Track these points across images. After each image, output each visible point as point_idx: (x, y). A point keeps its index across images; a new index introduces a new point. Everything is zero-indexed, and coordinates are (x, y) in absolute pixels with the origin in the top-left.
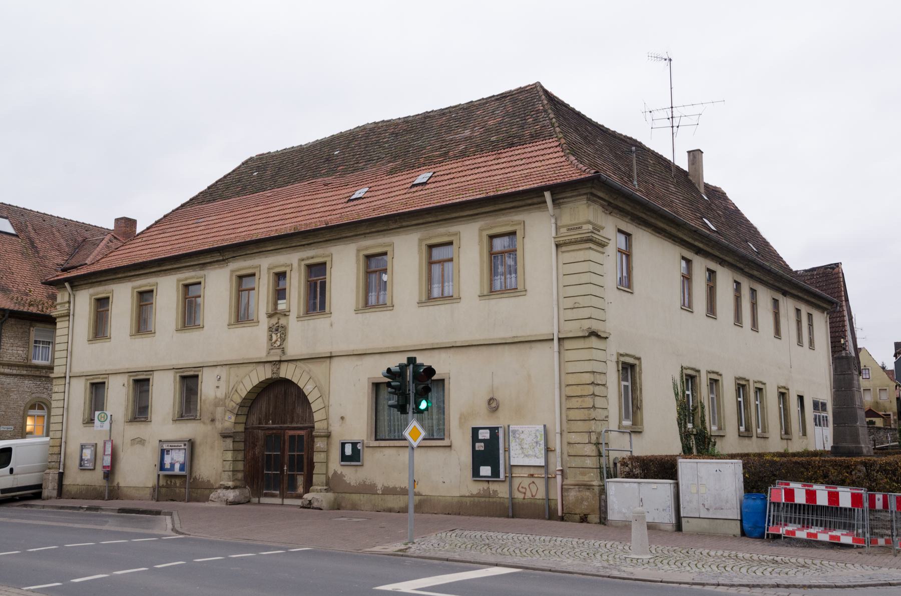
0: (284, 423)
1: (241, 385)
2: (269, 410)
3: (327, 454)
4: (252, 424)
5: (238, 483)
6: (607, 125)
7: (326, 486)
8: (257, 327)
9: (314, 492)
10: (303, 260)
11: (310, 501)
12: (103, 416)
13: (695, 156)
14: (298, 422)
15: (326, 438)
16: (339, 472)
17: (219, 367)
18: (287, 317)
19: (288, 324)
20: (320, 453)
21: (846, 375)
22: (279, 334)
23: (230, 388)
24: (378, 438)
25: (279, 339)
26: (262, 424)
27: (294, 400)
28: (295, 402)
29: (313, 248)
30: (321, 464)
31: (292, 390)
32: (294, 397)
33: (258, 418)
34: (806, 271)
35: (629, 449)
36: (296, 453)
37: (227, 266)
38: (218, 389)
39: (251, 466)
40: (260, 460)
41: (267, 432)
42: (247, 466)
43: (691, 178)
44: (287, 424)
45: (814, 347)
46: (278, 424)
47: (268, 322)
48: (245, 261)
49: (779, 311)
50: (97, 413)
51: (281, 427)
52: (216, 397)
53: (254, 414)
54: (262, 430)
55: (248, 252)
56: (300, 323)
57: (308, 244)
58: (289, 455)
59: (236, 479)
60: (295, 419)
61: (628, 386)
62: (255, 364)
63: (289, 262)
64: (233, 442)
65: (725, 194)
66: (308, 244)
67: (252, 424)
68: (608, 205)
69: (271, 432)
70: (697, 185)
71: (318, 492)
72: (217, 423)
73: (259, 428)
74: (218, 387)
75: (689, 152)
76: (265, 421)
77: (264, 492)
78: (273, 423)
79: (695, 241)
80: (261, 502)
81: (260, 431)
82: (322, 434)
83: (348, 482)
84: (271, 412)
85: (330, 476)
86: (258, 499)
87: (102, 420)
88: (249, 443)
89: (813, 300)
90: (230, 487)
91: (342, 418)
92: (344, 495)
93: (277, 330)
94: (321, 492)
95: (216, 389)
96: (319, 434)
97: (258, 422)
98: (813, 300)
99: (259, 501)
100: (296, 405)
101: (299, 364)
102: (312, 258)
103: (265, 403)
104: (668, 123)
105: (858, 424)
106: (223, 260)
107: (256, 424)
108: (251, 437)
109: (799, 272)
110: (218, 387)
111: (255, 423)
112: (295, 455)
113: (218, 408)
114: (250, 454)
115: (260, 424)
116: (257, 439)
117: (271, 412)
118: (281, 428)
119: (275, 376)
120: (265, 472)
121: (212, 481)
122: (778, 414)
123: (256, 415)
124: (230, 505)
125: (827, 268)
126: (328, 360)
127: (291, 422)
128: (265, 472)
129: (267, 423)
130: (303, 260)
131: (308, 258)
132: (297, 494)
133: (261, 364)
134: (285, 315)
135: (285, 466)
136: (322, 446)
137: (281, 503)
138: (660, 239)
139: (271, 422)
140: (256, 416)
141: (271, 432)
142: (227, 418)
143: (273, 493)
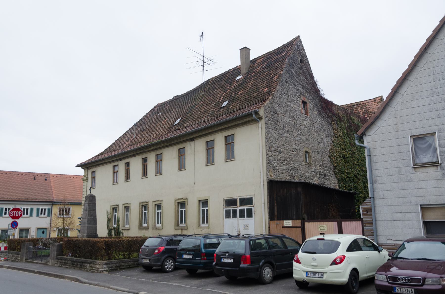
75: (240, 49)
89: (247, 120)
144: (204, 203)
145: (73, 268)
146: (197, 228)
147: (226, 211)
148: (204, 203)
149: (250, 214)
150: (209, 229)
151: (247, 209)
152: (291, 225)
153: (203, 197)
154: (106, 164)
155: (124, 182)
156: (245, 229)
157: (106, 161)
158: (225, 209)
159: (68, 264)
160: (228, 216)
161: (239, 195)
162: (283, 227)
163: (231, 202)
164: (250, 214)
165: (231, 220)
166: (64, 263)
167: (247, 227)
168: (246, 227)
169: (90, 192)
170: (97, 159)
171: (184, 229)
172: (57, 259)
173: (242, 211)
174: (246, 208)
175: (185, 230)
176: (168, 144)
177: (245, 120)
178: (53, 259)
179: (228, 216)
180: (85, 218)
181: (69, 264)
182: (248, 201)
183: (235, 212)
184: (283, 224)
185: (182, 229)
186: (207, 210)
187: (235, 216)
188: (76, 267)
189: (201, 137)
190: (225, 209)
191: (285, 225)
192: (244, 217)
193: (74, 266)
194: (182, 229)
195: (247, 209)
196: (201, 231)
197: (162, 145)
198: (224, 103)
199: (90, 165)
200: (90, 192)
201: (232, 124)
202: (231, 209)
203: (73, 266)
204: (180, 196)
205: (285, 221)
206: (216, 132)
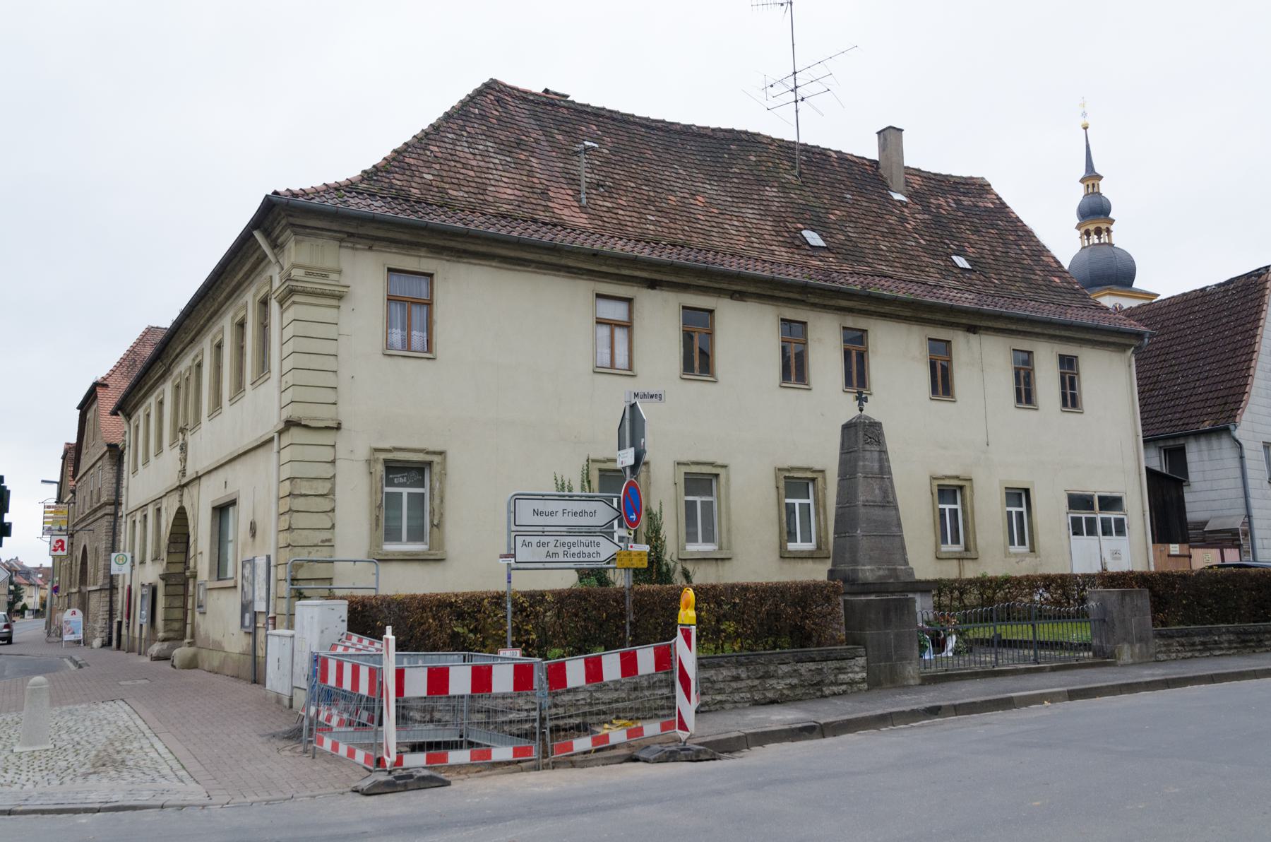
5: (171, 635)
6: (670, 118)
7: (378, 635)
12: (121, 558)
13: (890, 137)
21: (853, 454)
24: (221, 577)
34: (1219, 285)
35: (375, 587)
43: (882, 172)
45: (1082, 409)
49: (951, 357)
50: (114, 555)
59: (171, 630)
61: (423, 494)
64: (166, 585)
65: (989, 185)
68: (348, 236)
70: (889, 181)
75: (879, 133)
79: (618, 269)
87: (121, 562)
89: (1063, 333)
98: (1063, 333)
104: (792, 96)
105: (859, 532)
109: (1208, 289)
122: (1140, 513)
125: (1252, 276)
126: (197, 481)
144: (1019, 496)
145: (1248, 650)
146: (1005, 557)
147: (1072, 518)
148: (1019, 496)
149: (1121, 530)
150: (1038, 559)
151: (1115, 519)
152: (1178, 553)
153: (1019, 481)
154: (537, 268)
155: (778, 385)
156: (1115, 559)
157: (571, 263)
158: (1070, 515)
159: (1221, 643)
160: (1077, 529)
161: (1097, 487)
162: (1169, 556)
163: (1079, 502)
164: (1121, 530)
165: (1084, 541)
166: (1203, 643)
167: (1117, 555)
168: (1116, 554)
169: (861, 410)
170: (331, 202)
171: (967, 559)
172: (1161, 635)
173: (1105, 522)
174: (1112, 515)
175: (970, 561)
176: (908, 314)
177: (1112, 339)
178: (1141, 640)
179: (1077, 531)
180: (883, 506)
181: (1226, 645)
182: (1111, 503)
183: (1091, 522)
184: (1169, 550)
185: (959, 559)
186: (708, 507)
187: (1091, 532)
188: (1258, 647)
189: (998, 332)
190: (1070, 515)
191: (1172, 553)
192: (1111, 534)
193: (1251, 647)
194: (959, 559)
195: (1115, 519)
196: (1017, 563)
197: (887, 309)
198: (815, 235)
199: (752, 289)
200: (861, 410)
201: (1087, 337)
202: (1084, 515)
203: (1245, 647)
204: (949, 468)
205: (1171, 545)
206: (825, 307)
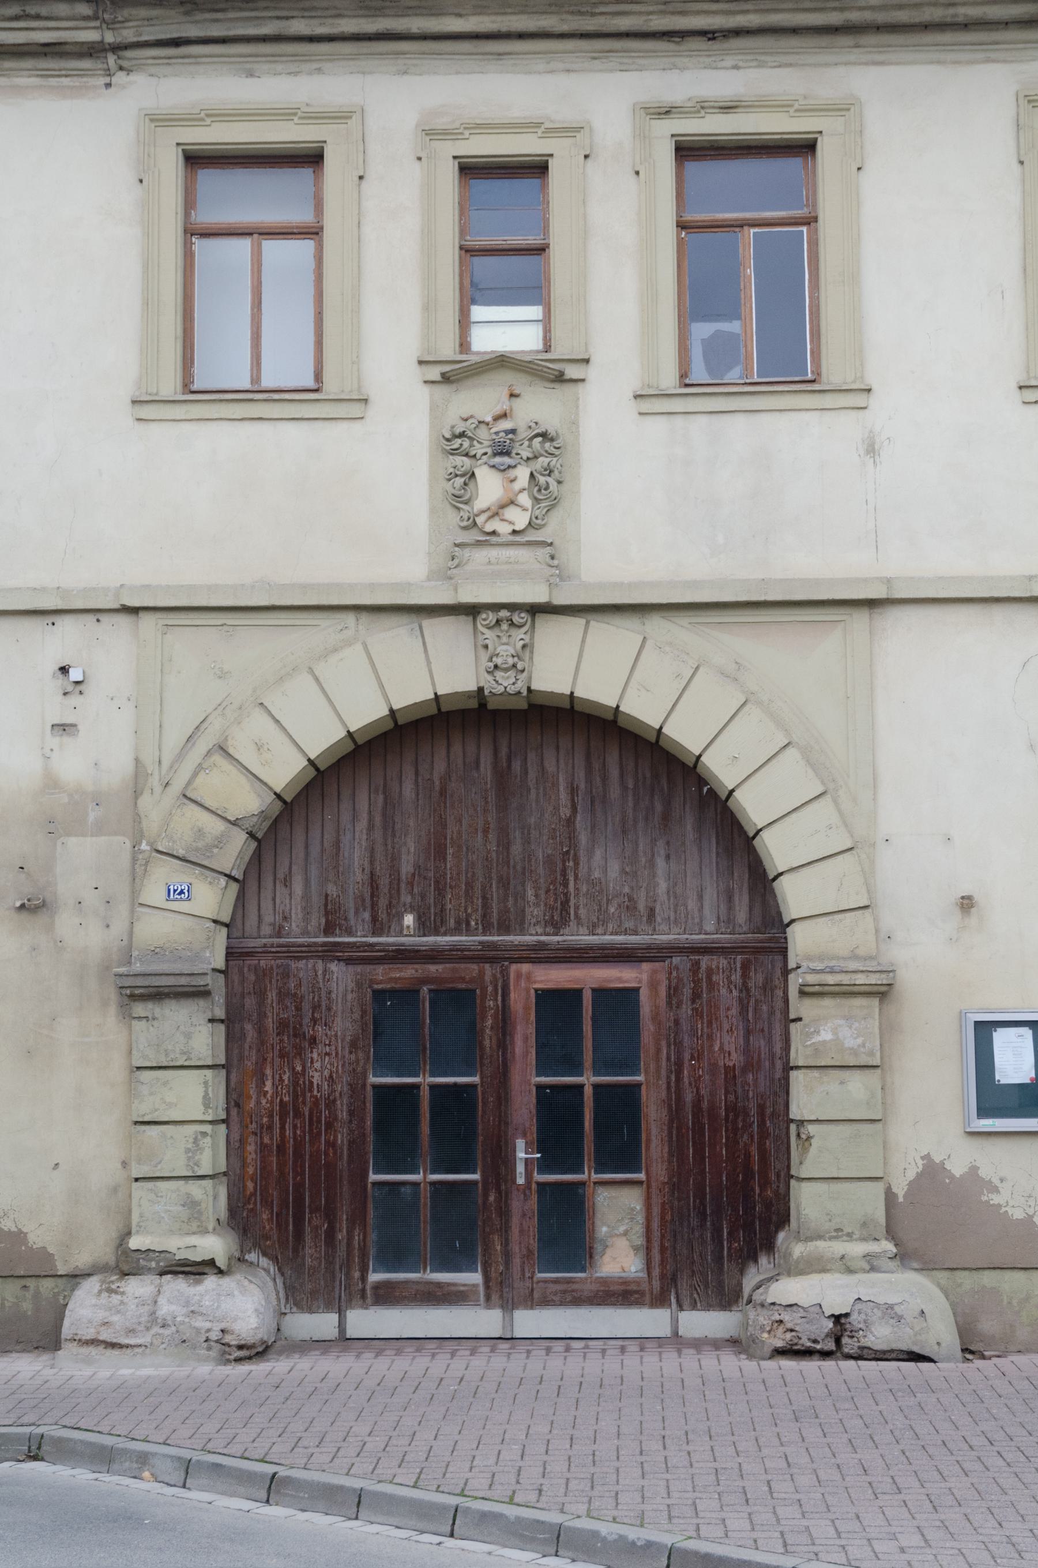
0: (505, 928)
1: (258, 725)
2: (394, 859)
3: (883, 1079)
4: (279, 933)
8: (357, 426)
9: (824, 1270)
10: (667, 112)
11: (837, 1319)
14: (605, 922)
15: (875, 1002)
16: (957, 1168)
17: (66, 624)
18: (568, 388)
19: (575, 423)
20: (846, 1074)
22: (522, 474)
23: (174, 738)
25: (524, 499)
26: (350, 932)
27: (565, 812)
28: (570, 822)
29: (729, 61)
30: (846, 1129)
31: (550, 766)
32: (564, 796)
33: (316, 900)
36: (425, 1080)
37: (108, 85)
38: (66, 739)
39: (281, 1149)
40: (343, 1115)
41: (380, 972)
42: (251, 1148)
44: (522, 932)
46: (462, 926)
47: (434, 408)
48: (251, 74)
51: (493, 946)
52: (51, 783)
53: (287, 882)
54: (349, 961)
55: (299, 26)
56: (658, 426)
57: (709, 35)
58: (540, 1087)
60: (582, 906)
62: (350, 618)
63: (563, 114)
66: (709, 35)
67: (279, 933)
69: (408, 972)
71: (850, 1271)
72: (66, 923)
73: (330, 952)
74: (63, 728)
76: (367, 915)
77: (374, 1277)
78: (424, 926)
80: (350, 1333)
81: (334, 967)
82: (861, 979)
83: (1018, 1214)
84: (406, 868)
85: (900, 1190)
86: (334, 1317)
88: (261, 1030)
90: (211, 1263)
91: (967, 904)
92: (988, 1279)
93: (502, 451)
94: (873, 1269)
95: (54, 741)
96: (845, 979)
97: (317, 920)
99: (675, 1322)
100: (583, 838)
101: (657, 626)
102: (727, 108)
103: (362, 824)
106: (92, 51)
107: (305, 933)
108: (272, 996)
110: (63, 728)
111: (295, 925)
112: (580, 1087)
113: (72, 841)
114: (268, 1087)
115: (328, 930)
116: (316, 1007)
117: (406, 868)
118: (490, 955)
119: (506, 683)
120: (373, 1177)
121: (38, 1237)
123: (298, 888)
124: (238, 1360)
127: (556, 925)
128: (373, 1177)
129: (377, 927)
130: (667, 112)
131: (702, 107)
132: (604, 1281)
133: (403, 619)
134: (560, 378)
135: (520, 1144)
136: (850, 1043)
137: (665, 1331)
138: (227, 171)
139: (409, 920)
140: (298, 888)
141: (408, 972)
142: (154, 893)
143: (439, 1285)
